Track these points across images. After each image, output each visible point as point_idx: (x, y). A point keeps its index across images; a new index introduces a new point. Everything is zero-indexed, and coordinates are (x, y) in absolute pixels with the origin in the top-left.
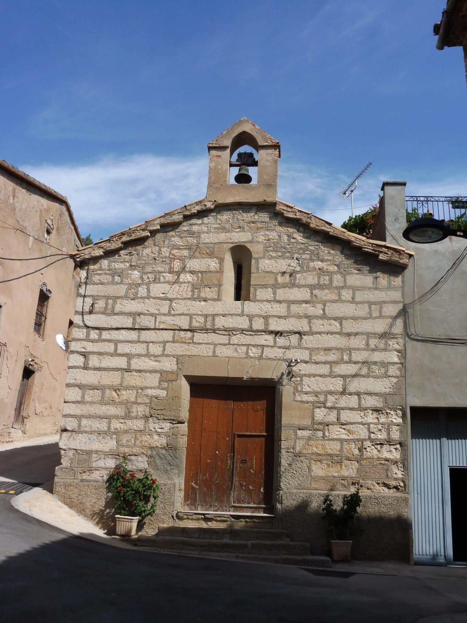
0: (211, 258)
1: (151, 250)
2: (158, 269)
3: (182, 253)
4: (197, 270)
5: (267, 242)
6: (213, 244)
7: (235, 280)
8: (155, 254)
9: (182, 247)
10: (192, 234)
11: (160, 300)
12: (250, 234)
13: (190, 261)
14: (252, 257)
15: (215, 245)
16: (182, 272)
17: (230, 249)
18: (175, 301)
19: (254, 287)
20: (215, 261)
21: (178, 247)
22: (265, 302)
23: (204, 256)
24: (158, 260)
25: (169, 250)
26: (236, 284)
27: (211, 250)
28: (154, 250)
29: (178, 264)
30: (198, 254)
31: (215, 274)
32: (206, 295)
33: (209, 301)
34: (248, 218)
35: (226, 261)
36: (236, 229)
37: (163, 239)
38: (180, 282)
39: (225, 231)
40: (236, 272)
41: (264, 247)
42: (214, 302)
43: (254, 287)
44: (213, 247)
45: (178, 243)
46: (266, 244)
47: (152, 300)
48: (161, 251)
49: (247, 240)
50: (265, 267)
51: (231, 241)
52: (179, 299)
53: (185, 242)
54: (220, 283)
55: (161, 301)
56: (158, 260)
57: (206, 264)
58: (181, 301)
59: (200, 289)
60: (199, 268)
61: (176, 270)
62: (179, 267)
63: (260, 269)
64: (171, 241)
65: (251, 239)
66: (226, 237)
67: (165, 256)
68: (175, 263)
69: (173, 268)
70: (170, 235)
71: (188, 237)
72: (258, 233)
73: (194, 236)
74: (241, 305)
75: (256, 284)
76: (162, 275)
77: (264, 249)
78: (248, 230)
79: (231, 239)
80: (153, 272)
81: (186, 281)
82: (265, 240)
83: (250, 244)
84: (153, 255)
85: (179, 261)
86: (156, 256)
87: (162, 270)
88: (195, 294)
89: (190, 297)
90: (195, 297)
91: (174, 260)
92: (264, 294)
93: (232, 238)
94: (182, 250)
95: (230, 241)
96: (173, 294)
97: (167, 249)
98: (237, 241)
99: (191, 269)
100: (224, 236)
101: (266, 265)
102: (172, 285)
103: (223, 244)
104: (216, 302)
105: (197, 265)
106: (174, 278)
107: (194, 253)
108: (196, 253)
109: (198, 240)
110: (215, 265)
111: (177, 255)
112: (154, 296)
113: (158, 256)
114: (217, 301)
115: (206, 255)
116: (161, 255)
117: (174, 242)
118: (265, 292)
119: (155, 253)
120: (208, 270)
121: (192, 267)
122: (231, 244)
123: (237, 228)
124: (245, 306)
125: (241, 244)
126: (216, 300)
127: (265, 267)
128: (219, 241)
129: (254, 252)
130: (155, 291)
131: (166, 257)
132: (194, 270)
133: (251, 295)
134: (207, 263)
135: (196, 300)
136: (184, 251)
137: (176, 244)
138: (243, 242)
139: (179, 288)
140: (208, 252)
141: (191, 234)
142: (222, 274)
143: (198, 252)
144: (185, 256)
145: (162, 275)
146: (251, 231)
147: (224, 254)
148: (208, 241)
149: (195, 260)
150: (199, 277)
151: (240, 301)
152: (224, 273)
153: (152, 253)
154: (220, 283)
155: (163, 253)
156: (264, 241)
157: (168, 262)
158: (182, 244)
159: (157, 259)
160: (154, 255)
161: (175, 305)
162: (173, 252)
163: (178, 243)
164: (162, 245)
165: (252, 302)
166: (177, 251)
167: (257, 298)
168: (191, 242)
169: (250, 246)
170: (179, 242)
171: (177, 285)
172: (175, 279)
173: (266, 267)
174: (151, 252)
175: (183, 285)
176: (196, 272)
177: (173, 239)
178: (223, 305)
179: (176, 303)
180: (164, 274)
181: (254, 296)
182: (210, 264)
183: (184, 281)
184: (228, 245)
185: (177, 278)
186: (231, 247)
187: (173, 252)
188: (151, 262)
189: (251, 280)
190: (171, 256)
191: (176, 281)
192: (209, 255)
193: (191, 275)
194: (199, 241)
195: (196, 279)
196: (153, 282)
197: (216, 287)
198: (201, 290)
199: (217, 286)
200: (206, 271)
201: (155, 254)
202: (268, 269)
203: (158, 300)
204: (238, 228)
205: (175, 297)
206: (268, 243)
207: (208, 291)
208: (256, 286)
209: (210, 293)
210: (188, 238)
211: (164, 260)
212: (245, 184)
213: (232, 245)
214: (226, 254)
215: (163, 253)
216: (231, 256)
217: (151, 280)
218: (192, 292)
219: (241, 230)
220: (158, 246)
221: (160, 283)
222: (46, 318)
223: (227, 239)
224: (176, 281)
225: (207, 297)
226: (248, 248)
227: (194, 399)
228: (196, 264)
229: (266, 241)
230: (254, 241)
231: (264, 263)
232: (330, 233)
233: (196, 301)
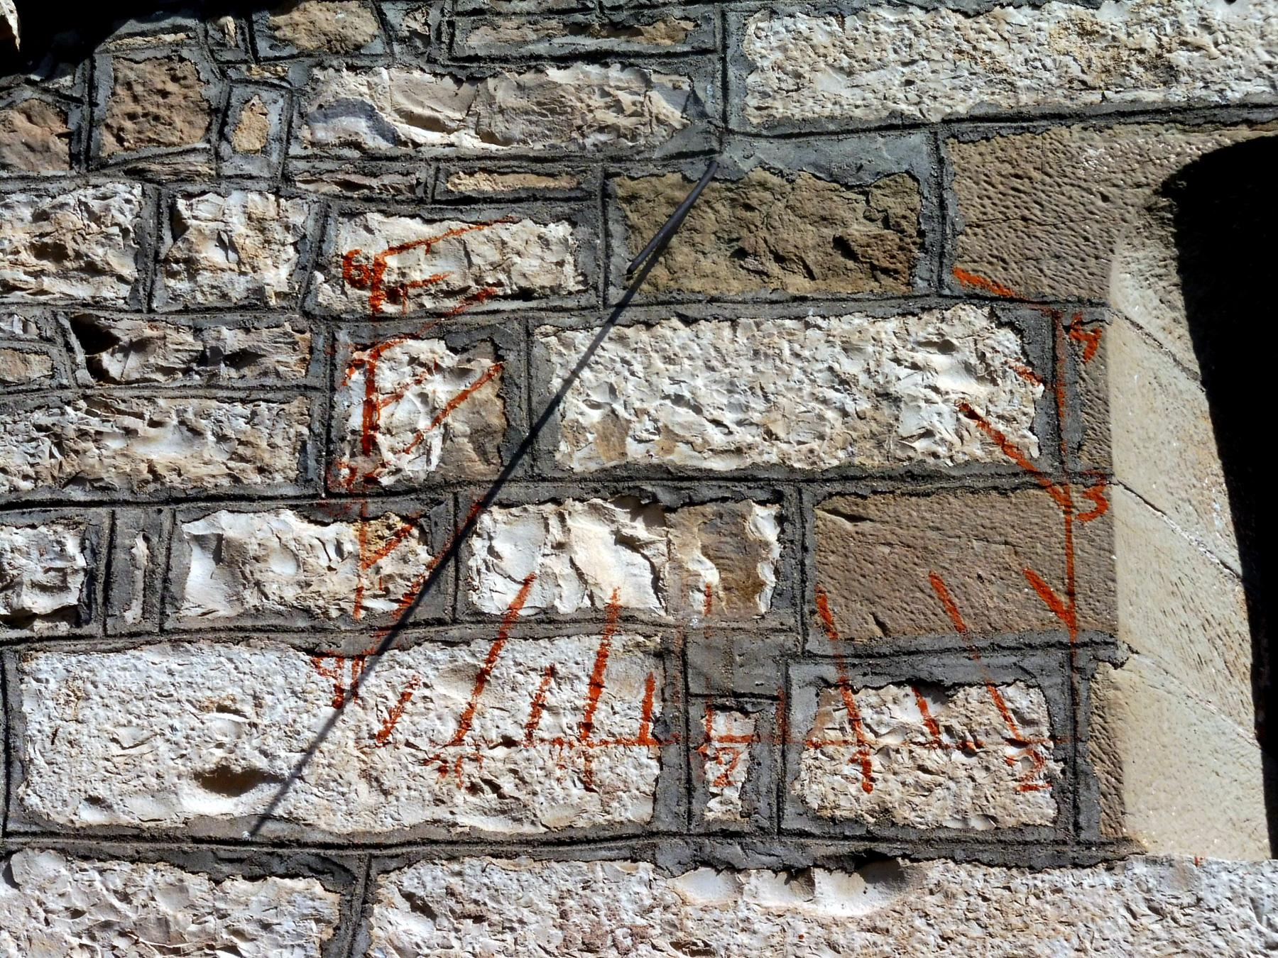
0: (910, 306)
1: (40, 216)
2: (140, 450)
3: (485, 253)
4: (720, 465)
6: (917, 139)
8: (92, 269)
9: (483, 184)
10: (616, 29)
11: (184, 863)
13: (610, 350)
15: (951, 152)
16: (511, 491)
17: (1167, 188)
18: (409, 879)
20: (976, 337)
21: (423, 174)
23: (798, 283)
24: (140, 346)
25: (299, 216)
27: (895, 206)
28: (75, 219)
29: (441, 389)
30: (717, 262)
31: (998, 511)
32: (891, 789)
33: (935, 871)
34: (1016, 288)
35: (1117, 338)
37: (213, 92)
38: (479, 616)
42: (1020, 881)
44: (925, 166)
45: (420, 134)
47: (48, 864)
48: (179, 227)
51: (1178, 94)
52: (474, 843)
53: (518, 128)
54: (1069, 616)
55: (197, 884)
56: (140, 346)
57: (844, 383)
58: (499, 874)
59: (783, 700)
60: (744, 436)
61: (414, 467)
62: (458, 423)
64: (328, 112)
66: (1096, 52)
67: (239, 288)
68: (387, 378)
69: (369, 446)
70: (306, 42)
71: (564, 61)
73: (637, 45)
76: (199, 528)
79: (1170, 74)
80: (77, 494)
81: (566, 607)
84: (56, 287)
85: (450, 360)
86: (111, 291)
87: (195, 469)
88: (713, 771)
89: (634, 811)
90: (715, 810)
91: (376, 347)
93: (1180, 58)
94: (489, 213)
95: (1152, 96)
96: (371, 778)
97: (263, 205)
99: (635, 451)
100: (1073, 42)
102: (365, 660)
103: (1057, 130)
104: (1044, 880)
105: (713, 398)
106: (388, 565)
107: (661, 248)
108: (682, 254)
109: (708, 91)
110: (976, 391)
111: (416, 276)
112: (91, 816)
113: (142, 301)
114: (1058, 863)
115: (833, 271)
116: (182, 285)
117: (360, 126)
119: (98, 254)
120: (873, 460)
121: (642, 427)
122: (1174, 137)
126: (1041, 855)
130: (96, 747)
131: (256, 303)
132: (681, 456)
134: (849, 367)
135: (733, 851)
136: (521, 232)
137: (383, 145)
139: (460, 696)
140: (858, 230)
141: (594, 19)
143: (709, 243)
144: (525, 294)
145: (199, 528)
147: (1102, 251)
148: (847, 95)
149: (675, 334)
150: (752, 549)
153: (56, 252)
154: (1069, 616)
155: (212, 254)
157: (286, 361)
158: (469, 142)
159: (126, 328)
160: (81, 291)
161: (414, 928)
162: (347, 239)
163: (420, 134)
164: (199, 164)
166: (410, 228)
168: (610, 117)
170: (432, 124)
171: (441, 655)
172: (400, 589)
174: (40, 251)
175: (518, 651)
176: (706, 491)
177: (352, 85)
179: (421, 907)
180: (230, 524)
182: (906, 383)
183: (536, 598)
184: (1130, 137)
185: (436, 572)
186: (1173, 163)
187: (347, 239)
188: (37, 369)
190: (327, 294)
191: (422, 613)
192: (875, 270)
193: (639, 530)
194: (712, 107)
195: (710, 575)
196: (63, 628)
197: (1028, 678)
198: (799, 715)
199: (1033, 661)
200: (845, 475)
201: (92, 269)
203: (151, 877)
205: (413, 815)
207: (903, 729)
209: (933, 758)
210: (554, 74)
211: (233, 340)
213: (1199, 144)
215: (212, 254)
216: (1177, 298)
217: (41, 603)
218: (673, 753)
220: (136, 174)
221: (179, 638)
222: (1117, 764)
223: (1115, 72)
224: (422, 613)
225: (904, 814)
228: (701, 385)
233: (732, 868)
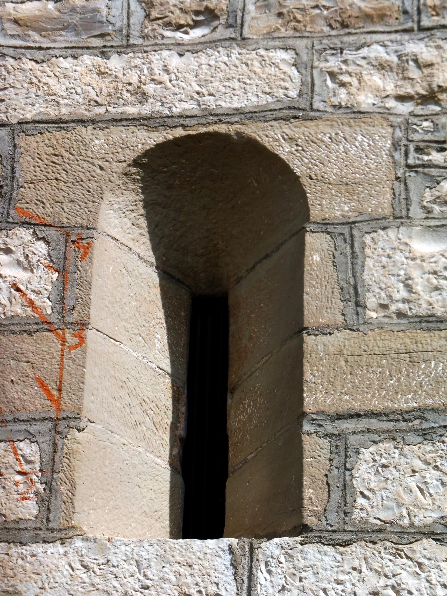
5: (419, 110)
7: (176, 400)
12: (288, 56)
14: (306, 216)
17: (136, 163)
19: (329, 428)
22: (428, 543)
26: (181, 431)
36: (179, 27)
39: (97, 42)
40: (184, 340)
41: (395, 145)
43: (329, 428)
46: (408, 126)
49: (266, 100)
50: (409, 288)
51: (146, 110)
54: (57, 402)
63: (371, 301)
65: (293, 93)
66: (105, 85)
72: (348, 55)
74: (235, 565)
75: (343, 407)
77: (398, 156)
78: (270, 35)
82: (401, 99)
83: (288, 129)
92: (412, 482)
93: (150, 88)
95: (132, 110)
98: (190, 107)
100: (93, 79)
101: (415, 274)
103: (80, 129)
104: (26, 550)
110: (21, 275)
118: (418, 464)
123: (188, 19)
124: (261, 576)
125: (222, 128)
126: (27, 535)
127: (409, 288)
128: (52, 112)
129: (322, 180)
133: (308, 492)
138: (238, 111)
142: (71, 340)
146: (290, 42)
151: (224, 542)
152: (90, 334)
154: (57, 402)
156: (391, 103)
165: (321, 540)
167: (357, 515)
169: (291, 139)
173: (419, 288)
178: (81, 573)
181: (336, 495)
186: (140, 149)
189: (308, 376)
197: (31, 437)
199: (35, 428)
202: (435, 297)
204: (196, 24)
206: (426, 117)
208: (348, 425)
212: (198, 542)
214: (108, 196)
216: (143, 222)
219: (217, 35)
226: (276, 159)
227: (224, 535)
229: (406, 108)
230: (317, 105)
231: (399, 257)
232: (266, 539)
